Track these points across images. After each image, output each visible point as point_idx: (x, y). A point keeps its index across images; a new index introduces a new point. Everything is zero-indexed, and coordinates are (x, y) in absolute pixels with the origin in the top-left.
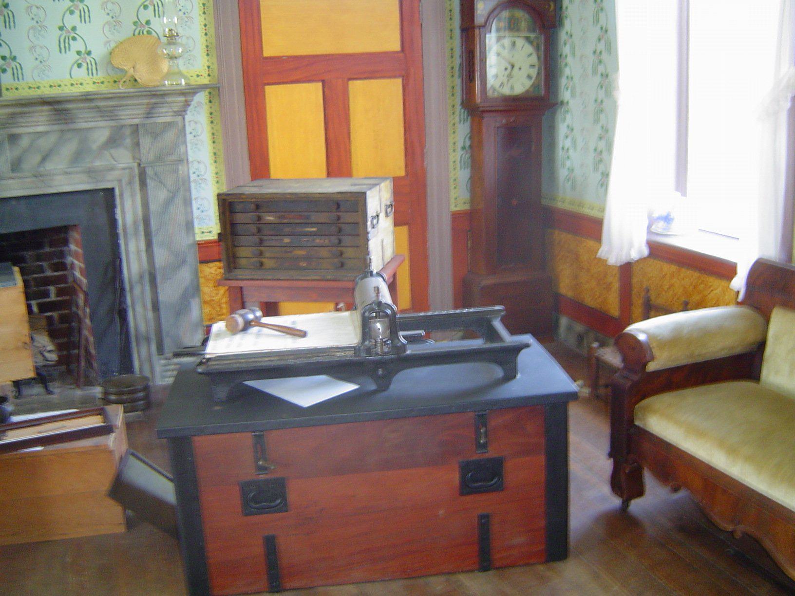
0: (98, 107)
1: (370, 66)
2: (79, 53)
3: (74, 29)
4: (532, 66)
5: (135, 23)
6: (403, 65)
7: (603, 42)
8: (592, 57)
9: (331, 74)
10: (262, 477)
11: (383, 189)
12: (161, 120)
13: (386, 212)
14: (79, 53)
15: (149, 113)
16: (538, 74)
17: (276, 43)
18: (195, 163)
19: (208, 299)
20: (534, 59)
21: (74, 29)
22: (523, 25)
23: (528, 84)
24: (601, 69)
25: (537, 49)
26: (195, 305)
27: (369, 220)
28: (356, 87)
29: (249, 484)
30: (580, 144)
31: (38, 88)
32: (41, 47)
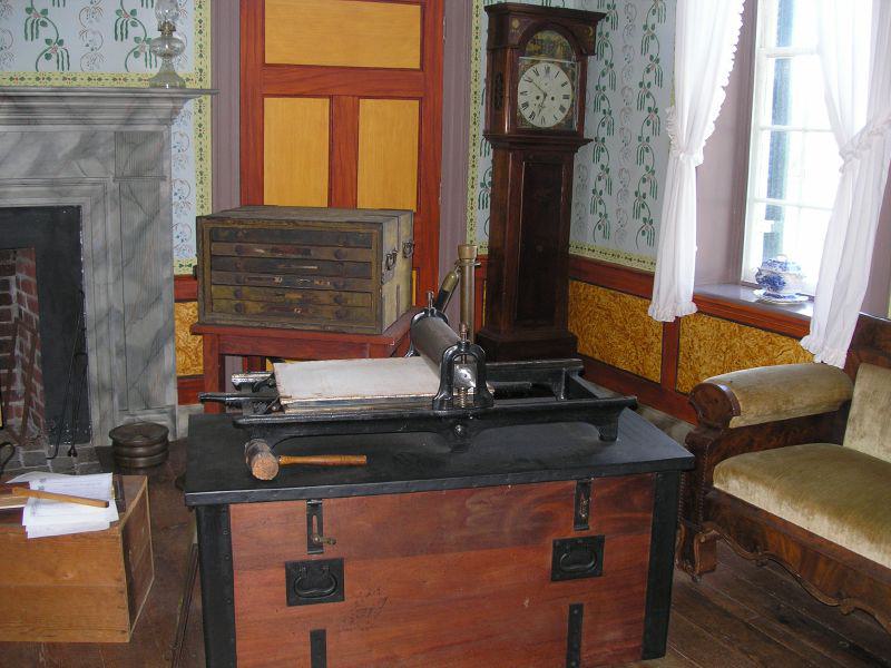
0: (68, 107)
1: (384, 83)
2: (48, 41)
3: (45, 12)
4: (566, 97)
5: (118, 12)
6: (421, 85)
7: (652, 72)
8: (637, 89)
9: (343, 89)
10: (315, 557)
11: (402, 223)
12: (142, 128)
13: (404, 253)
14: (48, 41)
15: (129, 119)
16: (572, 106)
17: (279, 49)
18: (178, 182)
19: (182, 344)
20: (568, 90)
21: (45, 12)
22: (559, 50)
23: (561, 116)
24: (649, 103)
25: (572, 78)
26: (168, 350)
27: (385, 259)
28: (367, 106)
29: (296, 565)
30: (617, 186)
31: (74, 79)
32: (94, 33)
